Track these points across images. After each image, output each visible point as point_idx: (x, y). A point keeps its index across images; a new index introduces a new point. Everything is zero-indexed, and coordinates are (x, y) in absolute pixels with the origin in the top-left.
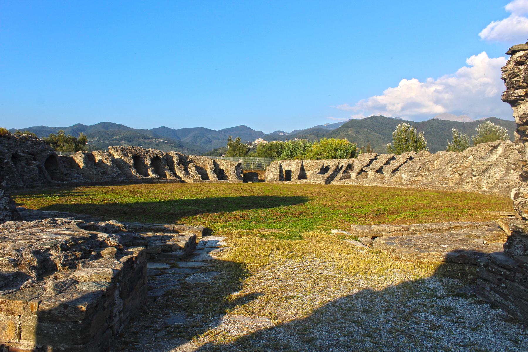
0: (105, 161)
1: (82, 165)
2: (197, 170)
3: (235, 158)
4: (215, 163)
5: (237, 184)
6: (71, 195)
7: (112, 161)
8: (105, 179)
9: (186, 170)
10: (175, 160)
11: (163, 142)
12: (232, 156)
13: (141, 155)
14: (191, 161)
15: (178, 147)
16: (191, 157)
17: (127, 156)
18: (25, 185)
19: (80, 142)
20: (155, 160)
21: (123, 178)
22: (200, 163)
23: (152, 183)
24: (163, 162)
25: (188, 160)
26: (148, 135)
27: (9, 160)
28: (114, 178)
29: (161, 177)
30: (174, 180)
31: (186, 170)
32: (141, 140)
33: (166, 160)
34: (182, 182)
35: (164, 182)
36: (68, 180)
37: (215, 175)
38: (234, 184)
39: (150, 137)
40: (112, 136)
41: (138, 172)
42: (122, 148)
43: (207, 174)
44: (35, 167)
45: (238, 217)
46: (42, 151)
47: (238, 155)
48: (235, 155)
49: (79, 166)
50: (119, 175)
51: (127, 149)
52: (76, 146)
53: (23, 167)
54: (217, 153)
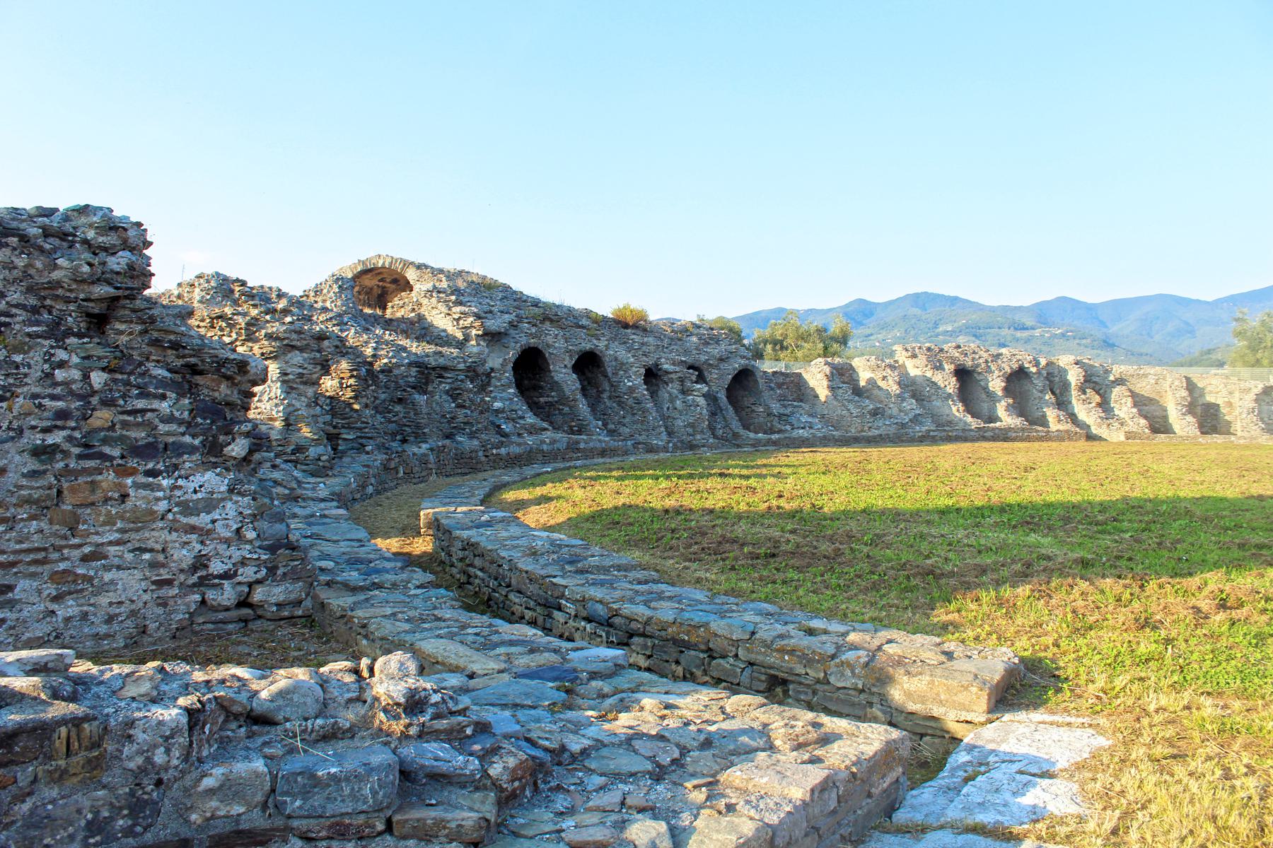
0: (880, 383)
1: (823, 393)
2: (1135, 405)
3: (1257, 370)
4: (1191, 386)
5: (1259, 447)
6: (730, 475)
7: (899, 384)
8: (878, 428)
9: (1104, 405)
10: (1074, 377)
11: (1063, 335)
12: (1247, 364)
13: (978, 365)
14: (1120, 381)
15: (1101, 348)
16: (1117, 370)
17: (939, 368)
18: (669, 442)
19: (834, 339)
20: (1017, 378)
21: (928, 426)
22: (1144, 388)
23: (1006, 439)
24: (1039, 383)
25: (1112, 378)
26: (1024, 320)
27: (639, 381)
28: (903, 426)
29: (1032, 423)
30: (1067, 431)
31: (1104, 405)
32: (1005, 332)
33: (1047, 378)
34: (1090, 437)
35: (1041, 439)
36: (786, 431)
37: (1190, 418)
38: (1247, 447)
39: (1029, 323)
40: (936, 325)
41: (969, 410)
42: (929, 349)
43: (1166, 417)
44: (698, 399)
45: (1205, 605)
46: (721, 360)
47: (1265, 362)
48: (1258, 363)
49: (817, 396)
50: (916, 420)
51: (941, 350)
52: (826, 348)
53: (672, 400)
54: (1210, 359)
